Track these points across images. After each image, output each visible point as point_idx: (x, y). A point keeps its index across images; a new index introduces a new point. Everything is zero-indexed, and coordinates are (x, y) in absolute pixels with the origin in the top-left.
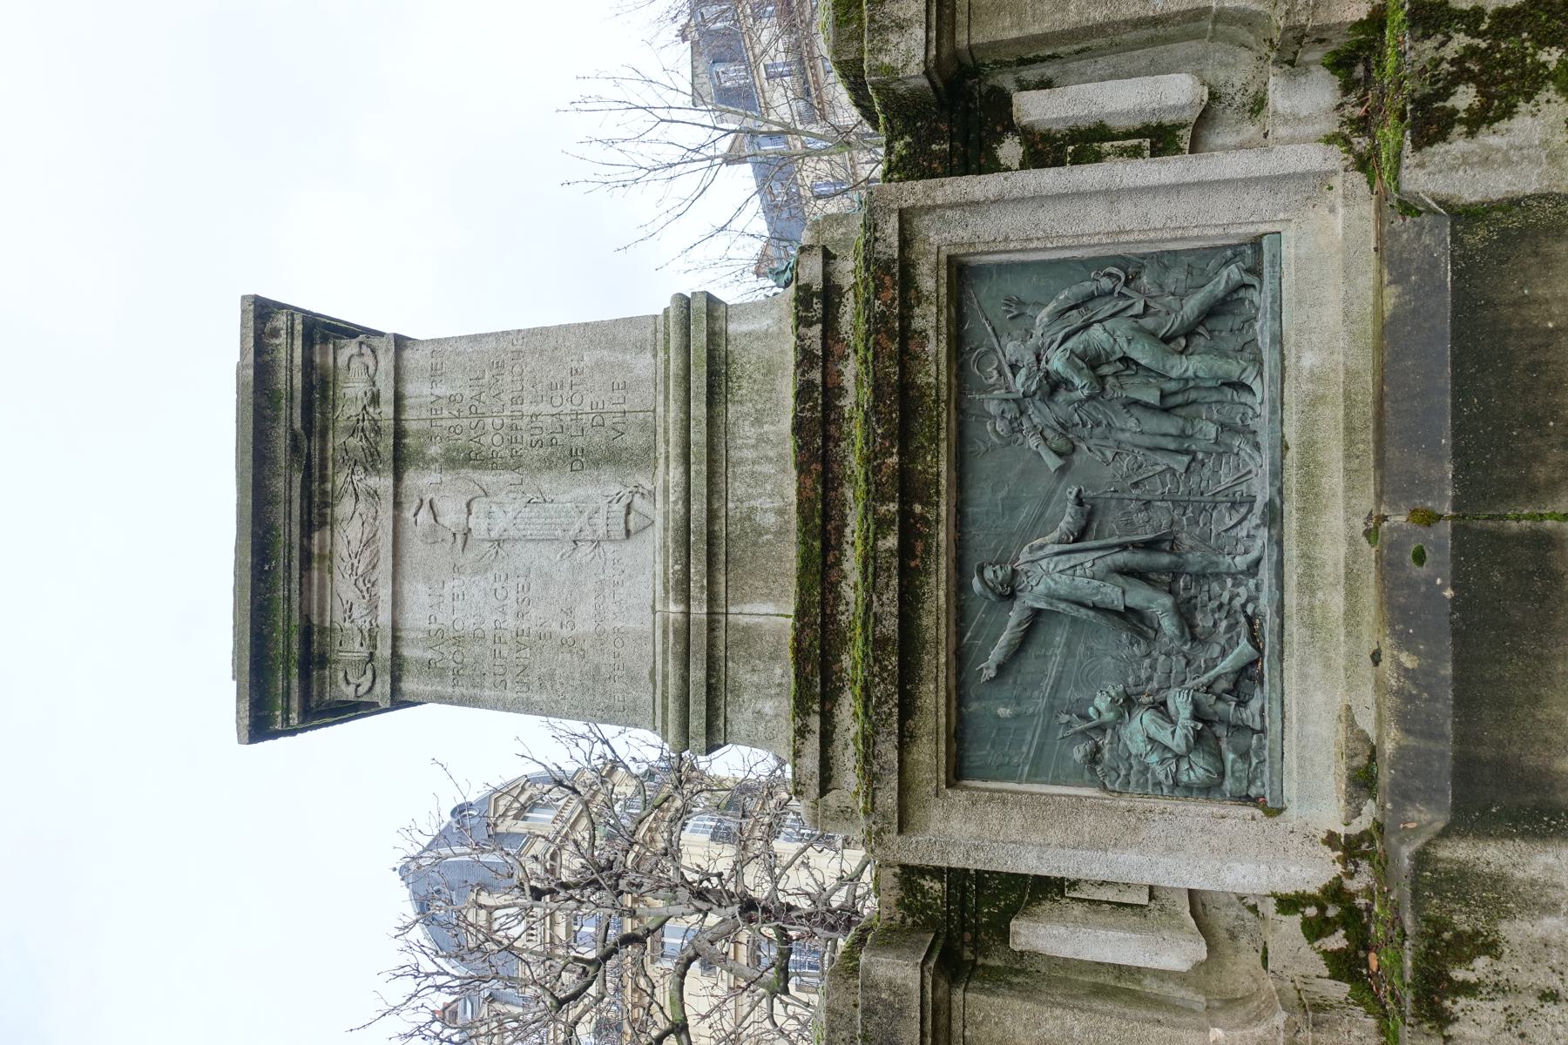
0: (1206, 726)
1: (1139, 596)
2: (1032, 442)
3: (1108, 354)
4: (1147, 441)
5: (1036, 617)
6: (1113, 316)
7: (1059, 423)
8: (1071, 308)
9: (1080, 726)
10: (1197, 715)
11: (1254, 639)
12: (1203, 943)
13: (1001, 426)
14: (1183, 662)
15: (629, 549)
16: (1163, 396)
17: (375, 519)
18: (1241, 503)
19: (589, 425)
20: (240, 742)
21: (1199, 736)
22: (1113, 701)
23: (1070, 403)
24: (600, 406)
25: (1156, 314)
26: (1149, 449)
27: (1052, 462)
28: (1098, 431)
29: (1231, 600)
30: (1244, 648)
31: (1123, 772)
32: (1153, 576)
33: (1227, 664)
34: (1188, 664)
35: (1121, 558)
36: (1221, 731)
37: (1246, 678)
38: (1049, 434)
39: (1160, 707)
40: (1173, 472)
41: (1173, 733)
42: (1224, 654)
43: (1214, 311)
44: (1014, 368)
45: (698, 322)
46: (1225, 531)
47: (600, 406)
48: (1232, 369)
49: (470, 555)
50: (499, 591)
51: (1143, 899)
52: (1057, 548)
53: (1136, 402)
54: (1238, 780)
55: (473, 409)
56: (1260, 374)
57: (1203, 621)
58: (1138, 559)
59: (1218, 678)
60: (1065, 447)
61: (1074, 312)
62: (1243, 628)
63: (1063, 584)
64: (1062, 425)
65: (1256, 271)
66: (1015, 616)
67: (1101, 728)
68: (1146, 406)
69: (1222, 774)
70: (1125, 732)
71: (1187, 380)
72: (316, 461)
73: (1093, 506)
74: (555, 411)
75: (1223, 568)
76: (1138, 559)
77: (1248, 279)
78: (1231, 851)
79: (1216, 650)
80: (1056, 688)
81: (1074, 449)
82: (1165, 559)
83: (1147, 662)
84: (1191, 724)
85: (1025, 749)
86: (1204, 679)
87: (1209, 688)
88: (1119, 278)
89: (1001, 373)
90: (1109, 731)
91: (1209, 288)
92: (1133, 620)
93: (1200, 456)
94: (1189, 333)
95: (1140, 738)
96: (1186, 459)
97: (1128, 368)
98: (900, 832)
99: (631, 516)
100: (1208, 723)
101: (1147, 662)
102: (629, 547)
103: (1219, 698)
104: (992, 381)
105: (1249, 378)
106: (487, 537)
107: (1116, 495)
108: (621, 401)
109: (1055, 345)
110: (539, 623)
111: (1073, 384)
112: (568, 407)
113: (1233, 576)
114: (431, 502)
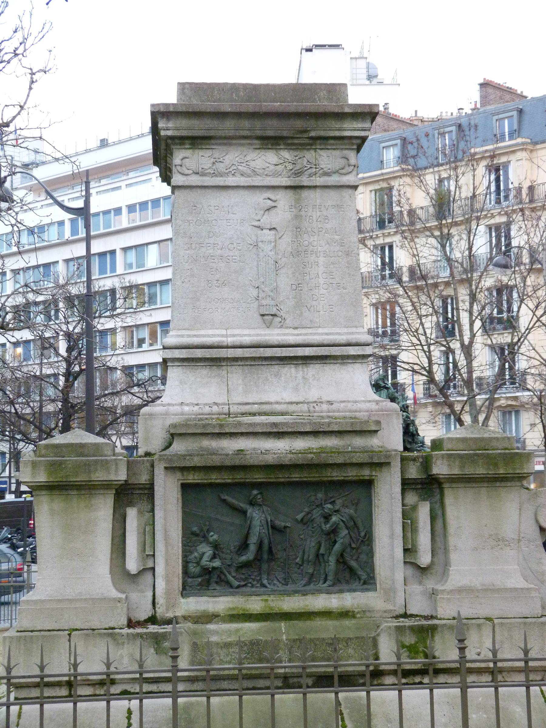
0: (207, 572)
1: (253, 548)
2: (306, 510)
3: (337, 536)
4: (307, 550)
5: (244, 513)
6: (351, 537)
7: (314, 519)
8: (354, 522)
9: (205, 529)
10: (214, 568)
11: (239, 587)
12: (136, 573)
13: (313, 498)
14: (229, 563)
15: (255, 315)
16: (323, 555)
17: (266, 175)
18: (285, 581)
19: (313, 293)
20: (153, 106)
21: (207, 569)
22: (216, 541)
23: (321, 523)
24: (322, 299)
25: (351, 551)
26: (304, 550)
27: (299, 517)
28: (311, 532)
29: (252, 579)
30: (236, 583)
31: (189, 544)
32: (259, 553)
33: (230, 578)
34: (229, 565)
35: (266, 542)
36: (207, 577)
38: (310, 515)
39: (214, 557)
40: (296, 559)
41: (207, 561)
42: (234, 577)
43: (351, 570)
44: (333, 503)
45: (363, 350)
46: (276, 577)
47: (322, 299)
48: (330, 578)
49: (249, 229)
50: (232, 246)
51: (149, 552)
52: (269, 520)
53: (320, 546)
54: (191, 582)
55: (320, 230)
56: (330, 586)
57: (244, 571)
58: (266, 547)
59: (225, 576)
60: (305, 520)
61: (353, 523)
62: (243, 583)
63: (256, 523)
64: (312, 520)
65: (365, 583)
66: (243, 505)
67: (204, 537)
68: (319, 549)
69: (193, 577)
70: (204, 545)
71: (328, 562)
72: (296, 141)
73: (283, 532)
74: (320, 274)
75: (263, 576)
76: (266, 547)
77: (362, 581)
78: (168, 581)
79: (234, 574)
80: (217, 519)
81: (305, 524)
82: (265, 556)
83: (228, 551)
84: (211, 567)
85: (194, 509)
86: (225, 571)
87: (222, 572)
88: (364, 539)
89: (331, 498)
90: (203, 539)
91: (360, 569)
92: (244, 546)
93: (302, 567)
94: (345, 563)
95: (204, 550)
96: (300, 563)
97: (333, 543)
98: (166, 468)
99: (271, 317)
100: (210, 572)
101: (228, 551)
102: (257, 315)
103: (219, 576)
104: (329, 494)
105: (328, 583)
106: (259, 240)
107: (288, 540)
108: (324, 310)
109: (341, 518)
110: (218, 268)
111: (327, 524)
112: (321, 281)
113: (260, 579)
114: (275, 207)
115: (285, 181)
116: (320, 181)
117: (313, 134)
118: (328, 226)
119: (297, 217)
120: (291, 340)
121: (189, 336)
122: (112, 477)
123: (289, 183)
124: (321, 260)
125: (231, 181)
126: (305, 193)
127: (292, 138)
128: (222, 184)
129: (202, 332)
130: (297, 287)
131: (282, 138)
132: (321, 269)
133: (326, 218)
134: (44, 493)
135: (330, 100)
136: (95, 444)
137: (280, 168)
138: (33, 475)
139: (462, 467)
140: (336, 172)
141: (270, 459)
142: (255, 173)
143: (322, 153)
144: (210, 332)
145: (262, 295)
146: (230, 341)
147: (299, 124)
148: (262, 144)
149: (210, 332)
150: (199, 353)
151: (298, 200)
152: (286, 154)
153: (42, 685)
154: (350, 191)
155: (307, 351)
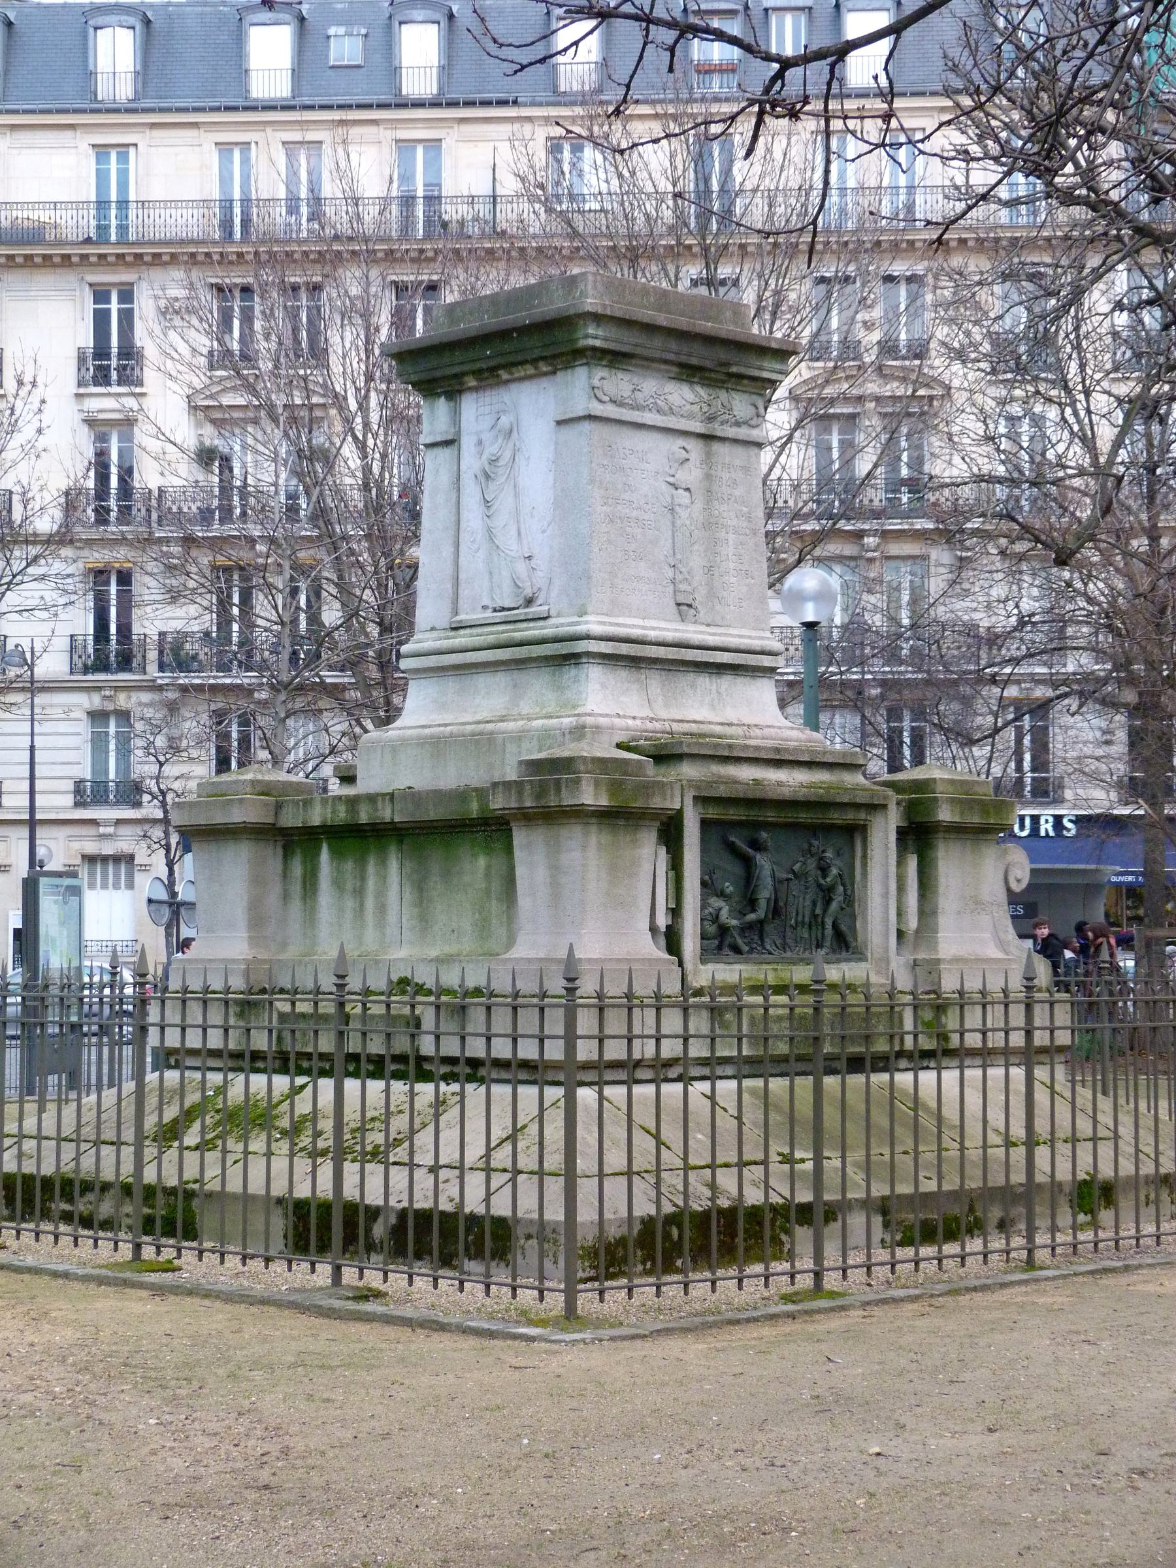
37: (737, 950)
49: (664, 487)
72: (713, 375)
102: (672, 603)
115: (698, 427)
116: (732, 432)
117: (734, 369)
118: (737, 493)
119: (708, 477)
120: (711, 640)
121: (611, 624)
122: (668, 805)
123: (703, 431)
124: (731, 537)
125: (649, 418)
126: (716, 447)
127: (711, 370)
128: (639, 420)
129: (621, 620)
130: (709, 569)
131: (701, 369)
132: (731, 550)
133: (735, 482)
134: (594, 820)
135: (736, 324)
136: (616, 760)
137: (696, 408)
138: (596, 795)
139: (962, 813)
140: (745, 423)
141: (786, 793)
142: (672, 412)
143: (733, 394)
144: (629, 621)
145: (679, 577)
146: (652, 635)
147: (723, 354)
148: (680, 374)
149: (629, 621)
150: (624, 649)
151: (708, 454)
152: (702, 391)
153: (714, 1062)
154: (756, 450)
155: (725, 658)
